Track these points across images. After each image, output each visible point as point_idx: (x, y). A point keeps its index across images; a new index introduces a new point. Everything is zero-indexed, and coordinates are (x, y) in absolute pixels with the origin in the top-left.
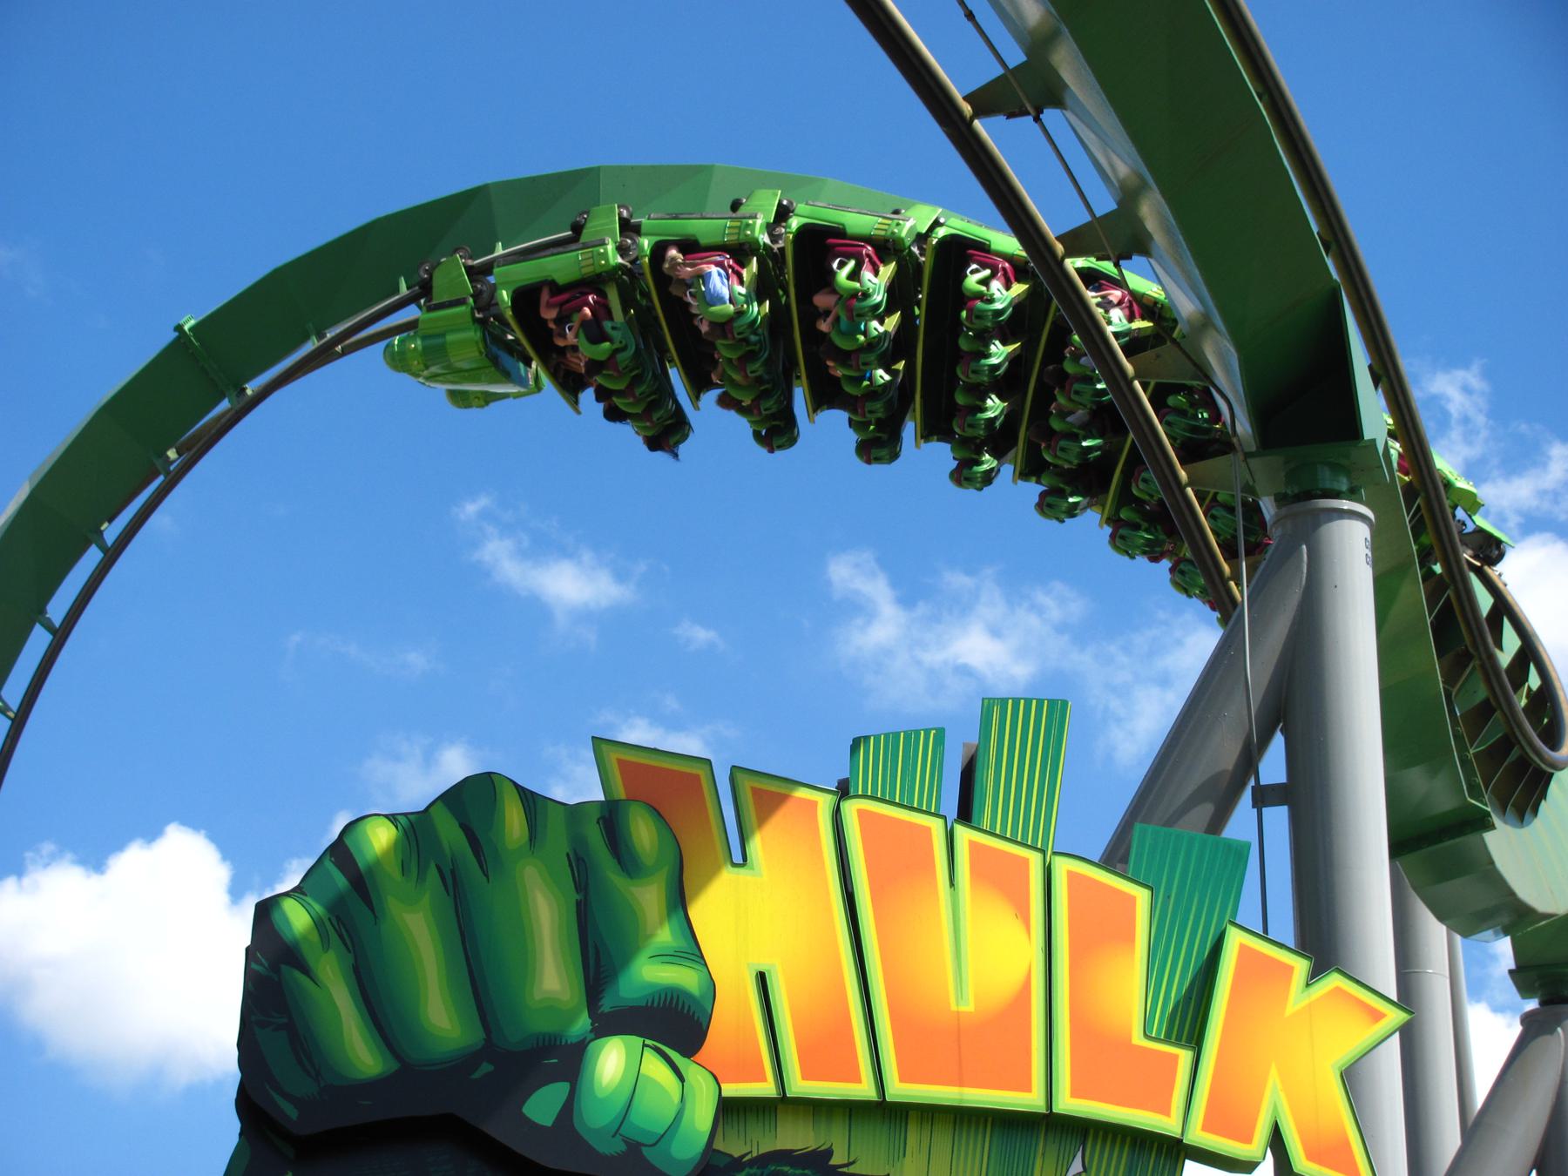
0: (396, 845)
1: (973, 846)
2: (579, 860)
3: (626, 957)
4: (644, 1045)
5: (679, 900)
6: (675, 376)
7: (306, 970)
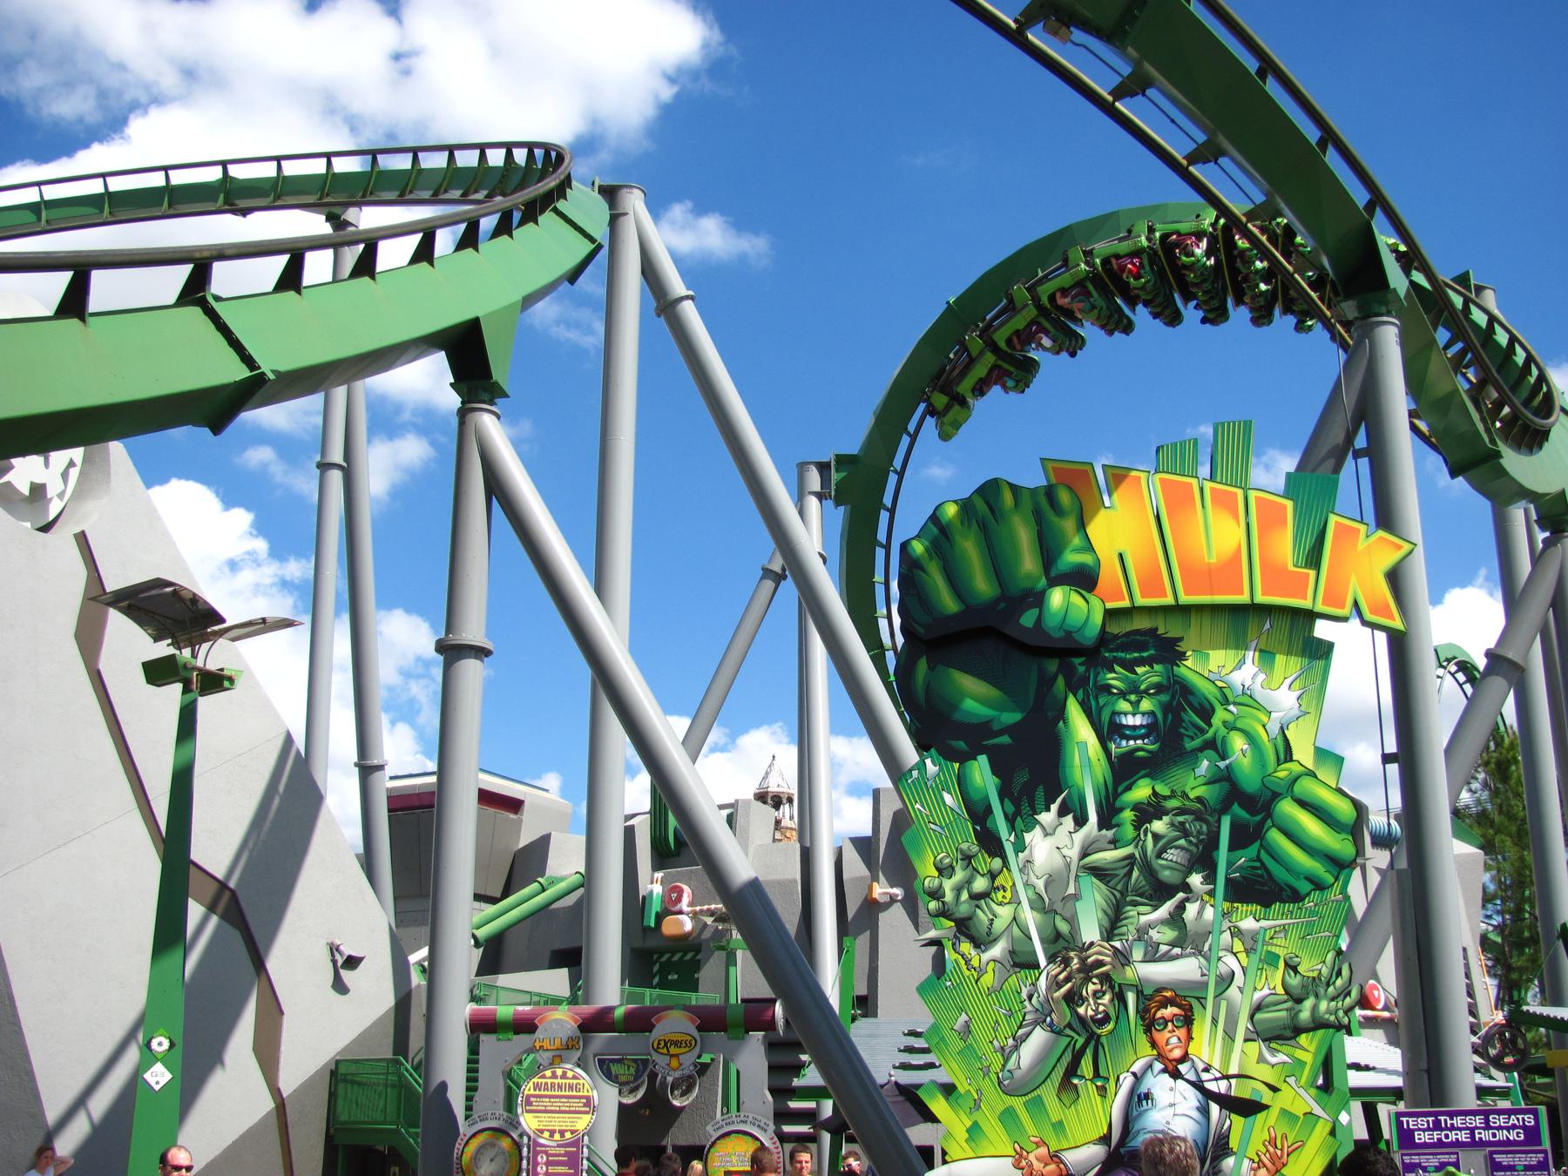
0: (958, 513)
1: (1212, 489)
3: (1060, 551)
5: (1082, 525)
6: (1177, 296)
7: (923, 569)
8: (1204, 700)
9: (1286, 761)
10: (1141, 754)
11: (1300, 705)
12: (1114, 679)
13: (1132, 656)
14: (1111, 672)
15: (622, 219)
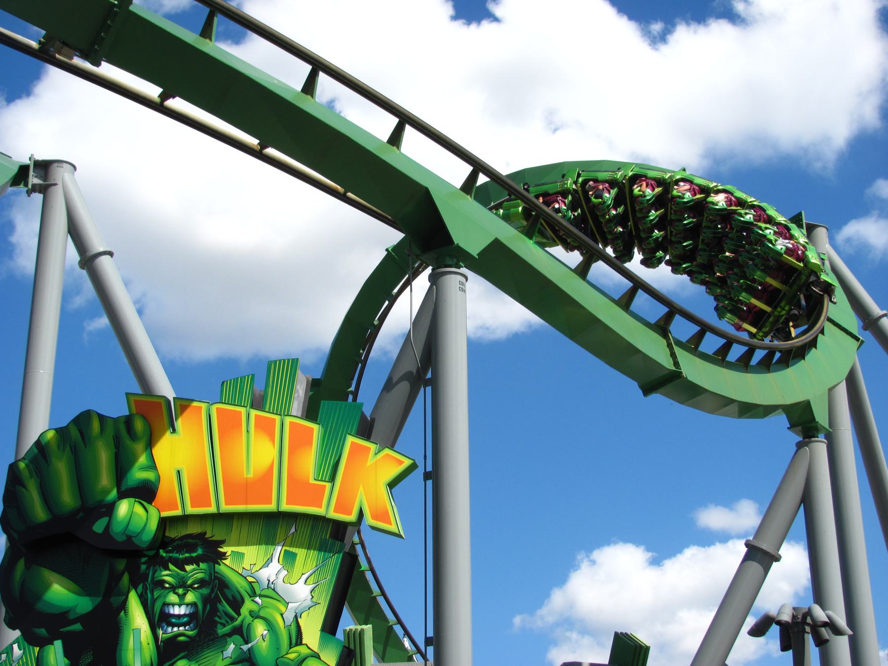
2: (116, 437)
4: (135, 501)
5: (150, 444)
7: (24, 486)
8: (236, 591)
9: (297, 645)
10: (182, 638)
11: (313, 597)
12: (167, 576)
13: (184, 556)
14: (166, 570)
15: (53, 188)
